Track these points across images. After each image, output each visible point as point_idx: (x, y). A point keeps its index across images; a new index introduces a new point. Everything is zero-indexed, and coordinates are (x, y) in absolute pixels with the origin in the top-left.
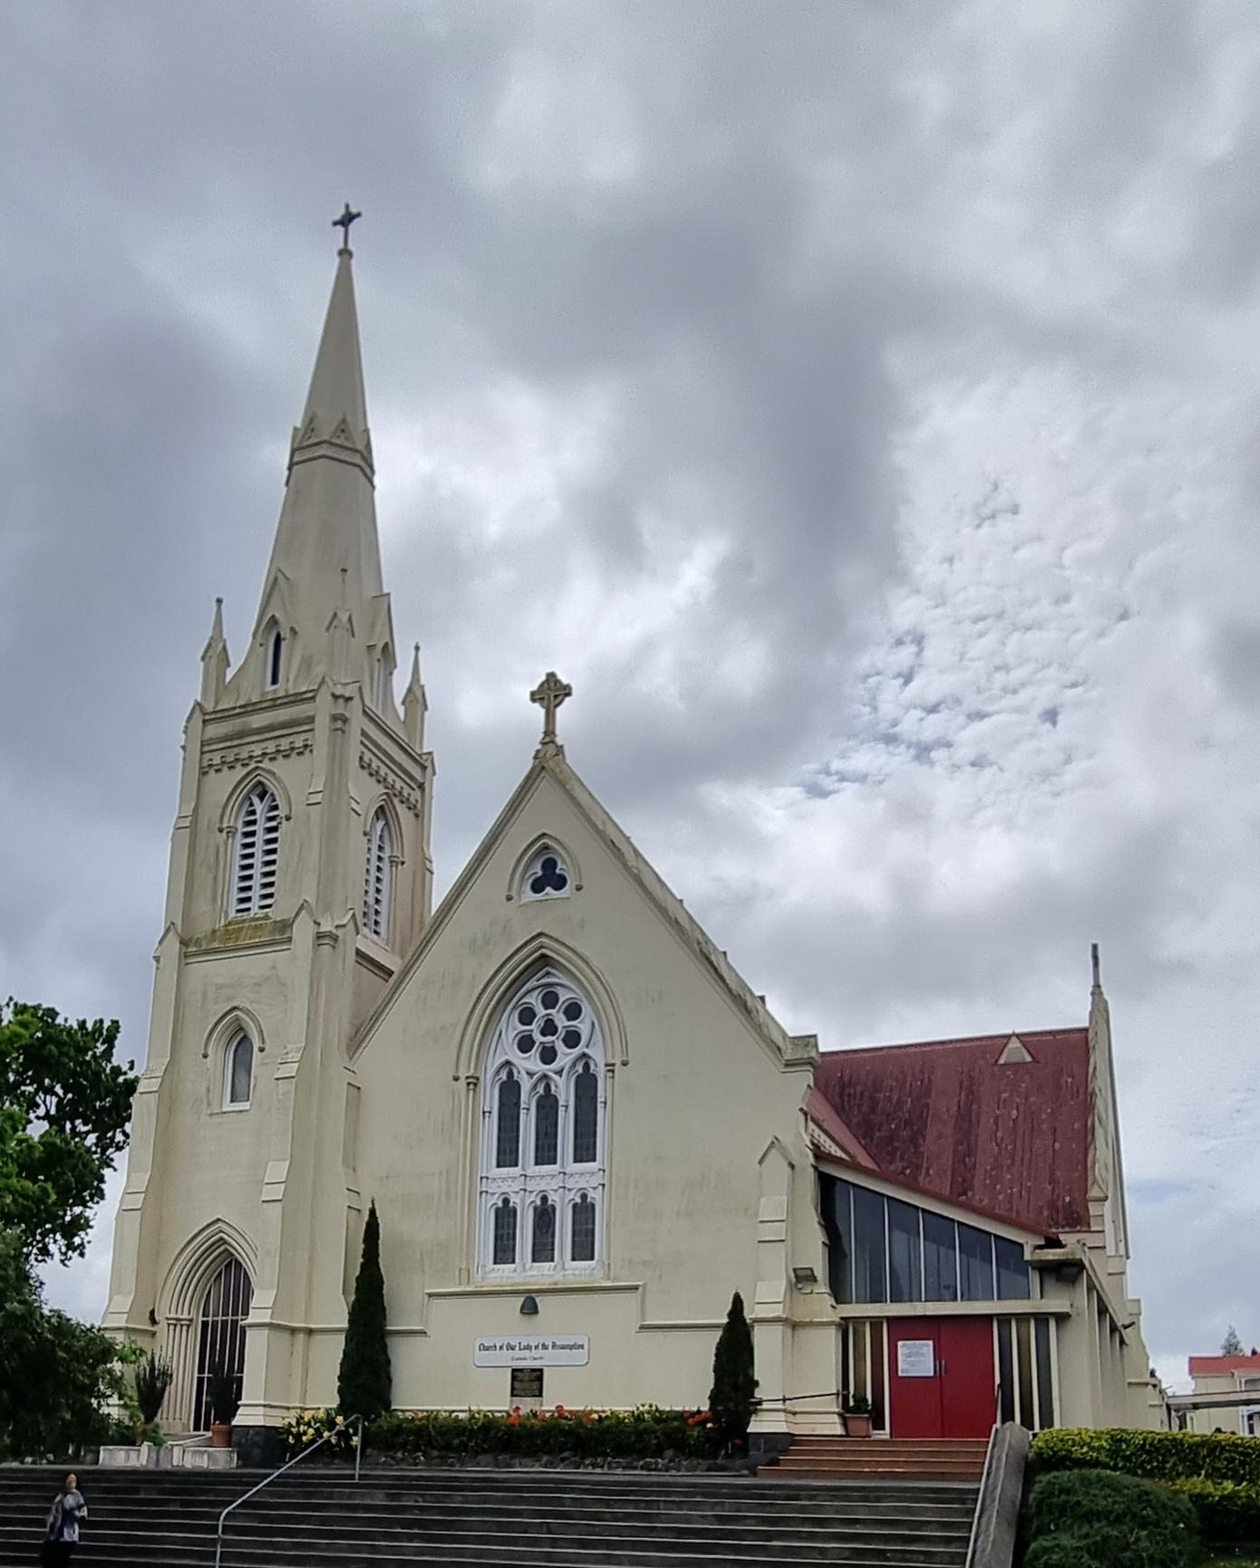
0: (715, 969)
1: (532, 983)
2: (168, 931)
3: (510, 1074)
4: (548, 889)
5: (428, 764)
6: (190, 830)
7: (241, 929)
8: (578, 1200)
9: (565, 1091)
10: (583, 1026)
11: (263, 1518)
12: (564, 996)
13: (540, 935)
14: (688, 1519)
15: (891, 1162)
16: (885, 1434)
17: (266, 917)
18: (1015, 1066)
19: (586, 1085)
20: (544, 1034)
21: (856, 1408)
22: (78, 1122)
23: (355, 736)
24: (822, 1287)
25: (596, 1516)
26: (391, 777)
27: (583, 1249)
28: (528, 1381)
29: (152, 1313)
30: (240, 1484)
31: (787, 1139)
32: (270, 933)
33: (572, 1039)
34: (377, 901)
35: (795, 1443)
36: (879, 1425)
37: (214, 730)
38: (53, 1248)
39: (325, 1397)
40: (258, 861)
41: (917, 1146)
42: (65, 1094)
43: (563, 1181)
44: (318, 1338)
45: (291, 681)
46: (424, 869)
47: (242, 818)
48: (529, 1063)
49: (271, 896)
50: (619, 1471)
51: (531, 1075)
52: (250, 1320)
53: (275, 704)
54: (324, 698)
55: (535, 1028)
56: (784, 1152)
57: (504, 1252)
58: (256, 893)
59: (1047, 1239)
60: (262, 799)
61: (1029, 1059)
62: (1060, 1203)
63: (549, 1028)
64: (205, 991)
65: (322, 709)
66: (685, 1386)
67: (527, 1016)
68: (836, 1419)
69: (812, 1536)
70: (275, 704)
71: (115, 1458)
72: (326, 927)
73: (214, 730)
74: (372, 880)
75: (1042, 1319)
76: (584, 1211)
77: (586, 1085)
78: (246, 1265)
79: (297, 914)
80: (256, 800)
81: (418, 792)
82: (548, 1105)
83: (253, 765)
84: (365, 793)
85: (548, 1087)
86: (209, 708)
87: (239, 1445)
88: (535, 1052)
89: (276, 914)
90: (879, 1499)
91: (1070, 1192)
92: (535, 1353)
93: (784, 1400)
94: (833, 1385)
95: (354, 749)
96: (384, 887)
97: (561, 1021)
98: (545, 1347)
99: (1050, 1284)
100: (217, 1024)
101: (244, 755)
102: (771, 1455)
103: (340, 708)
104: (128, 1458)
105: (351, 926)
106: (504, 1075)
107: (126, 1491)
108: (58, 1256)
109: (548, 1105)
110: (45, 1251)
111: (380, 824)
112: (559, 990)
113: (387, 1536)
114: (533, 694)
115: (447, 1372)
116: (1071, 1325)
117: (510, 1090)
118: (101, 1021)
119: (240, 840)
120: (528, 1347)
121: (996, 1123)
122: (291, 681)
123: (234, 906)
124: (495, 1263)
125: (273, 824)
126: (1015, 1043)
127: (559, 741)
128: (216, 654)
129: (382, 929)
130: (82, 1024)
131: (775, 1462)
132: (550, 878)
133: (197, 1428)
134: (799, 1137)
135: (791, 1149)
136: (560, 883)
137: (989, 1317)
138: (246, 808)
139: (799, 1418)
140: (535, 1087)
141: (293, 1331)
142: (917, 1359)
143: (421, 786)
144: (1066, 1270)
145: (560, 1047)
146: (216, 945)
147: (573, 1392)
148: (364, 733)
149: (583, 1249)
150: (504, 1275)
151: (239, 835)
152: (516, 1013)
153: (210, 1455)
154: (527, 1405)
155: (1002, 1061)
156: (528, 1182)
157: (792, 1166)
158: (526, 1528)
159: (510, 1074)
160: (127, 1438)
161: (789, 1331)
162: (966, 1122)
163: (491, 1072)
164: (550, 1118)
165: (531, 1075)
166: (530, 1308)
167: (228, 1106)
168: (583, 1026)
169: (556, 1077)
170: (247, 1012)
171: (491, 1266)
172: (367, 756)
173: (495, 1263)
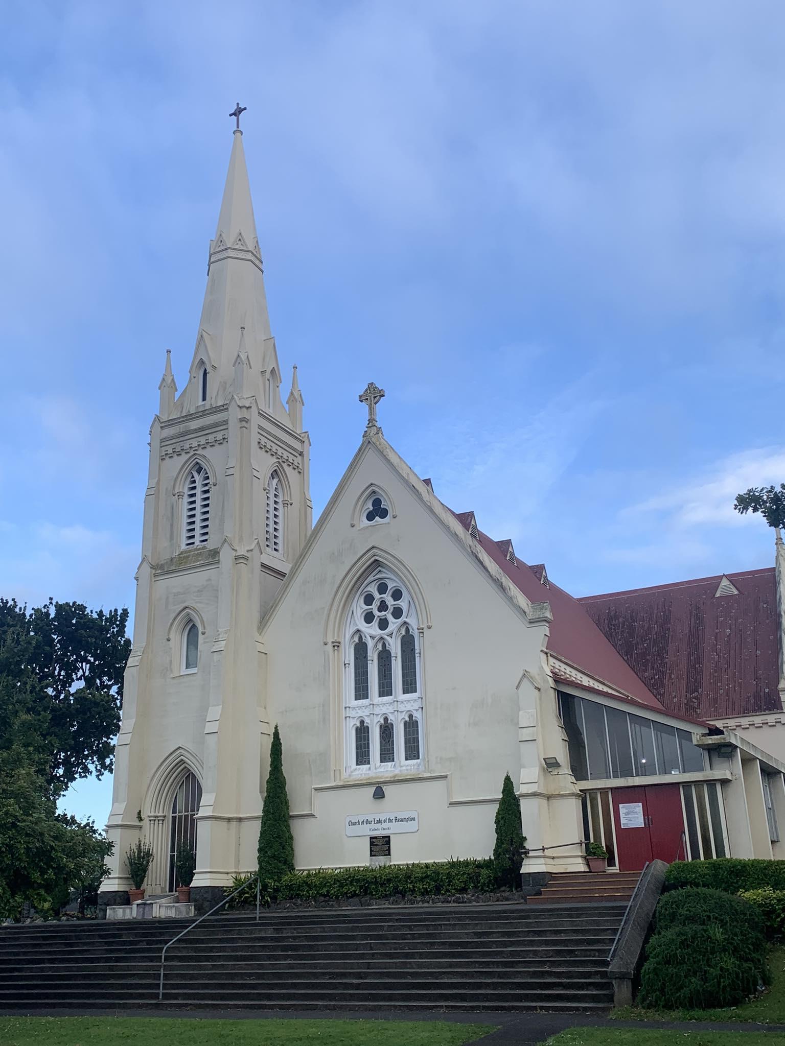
0: (481, 563)
1: (371, 578)
2: (143, 560)
3: (360, 638)
4: (377, 518)
5: (305, 440)
6: (153, 494)
7: (188, 557)
8: (407, 719)
9: (395, 647)
10: (403, 603)
11: (196, 950)
12: (391, 585)
13: (373, 547)
14: (457, 936)
15: (645, 671)
16: (615, 869)
17: (204, 548)
18: (728, 598)
19: (408, 644)
20: (380, 610)
21: (591, 852)
22: (105, 678)
23: (255, 429)
24: (566, 769)
25: (403, 937)
26: (280, 451)
27: (412, 752)
28: (380, 845)
29: (139, 813)
30: (176, 927)
31: (534, 671)
32: (207, 558)
33: (397, 613)
34: (276, 530)
35: (555, 879)
36: (611, 863)
37: (168, 432)
38: (91, 767)
39: (250, 864)
40: (198, 512)
41: (662, 658)
42: (95, 661)
43: (398, 706)
44: (245, 824)
45: (215, 398)
46: (306, 506)
47: (188, 485)
48: (372, 630)
49: (207, 533)
50: (439, 904)
51: (372, 637)
52: (201, 813)
53: (204, 413)
54: (233, 409)
55: (374, 607)
56: (531, 680)
57: (362, 757)
58: (198, 532)
59: (709, 729)
60: (199, 473)
61: (736, 592)
62: (762, 694)
63: (383, 607)
64: (167, 598)
65: (234, 414)
66: (476, 842)
67: (369, 600)
68: (580, 860)
69: (532, 943)
70: (204, 413)
71: (117, 913)
72: (242, 551)
73: (168, 432)
74: (271, 516)
75: (711, 783)
76: (411, 726)
77: (408, 644)
78: (199, 777)
79: (222, 545)
80: (195, 474)
81: (300, 458)
82: (385, 657)
83: (192, 453)
84: (264, 464)
85: (384, 645)
86: (165, 418)
87: (195, 900)
88: (375, 623)
89: (210, 545)
90: (578, 916)
91: (768, 686)
92: (385, 825)
93: (543, 849)
94: (576, 835)
95: (255, 437)
96: (280, 520)
97: (390, 602)
98: (390, 821)
99: (716, 759)
100: (175, 619)
101: (187, 446)
102: (537, 888)
103: (245, 414)
104: (124, 912)
105: (256, 551)
106: (356, 639)
107: (114, 936)
108: (95, 773)
109: (385, 657)
110: (86, 770)
111: (276, 480)
112: (388, 582)
113: (269, 958)
114: (360, 397)
115: (331, 843)
116: (731, 788)
117: (361, 649)
118: (116, 610)
119: (186, 499)
120: (379, 822)
121: (716, 638)
122: (215, 398)
123: (185, 541)
124: (357, 764)
125: (206, 488)
126: (725, 582)
127: (378, 425)
128: (167, 385)
129: (280, 547)
130: (101, 614)
131: (540, 893)
132: (378, 511)
133: (171, 890)
134: (544, 667)
135: (537, 677)
136: (383, 513)
137: (676, 785)
138: (189, 479)
139: (557, 861)
140: (376, 645)
141: (229, 820)
142: (633, 816)
143: (301, 454)
144: (723, 750)
145: (390, 618)
146: (173, 568)
147: (405, 854)
148: (260, 427)
149: (412, 752)
150: (363, 772)
151: (186, 496)
152: (363, 597)
153: (176, 908)
154: (381, 861)
155: (717, 595)
156: (377, 708)
157: (539, 690)
158: (357, 947)
159: (360, 638)
160: (124, 899)
161: (545, 801)
162: (695, 640)
163: (348, 637)
164: (388, 665)
165: (372, 637)
166: (379, 794)
167: (184, 671)
168: (403, 603)
169: (388, 638)
170: (194, 609)
171: (354, 766)
172: (263, 440)
173: (357, 764)
